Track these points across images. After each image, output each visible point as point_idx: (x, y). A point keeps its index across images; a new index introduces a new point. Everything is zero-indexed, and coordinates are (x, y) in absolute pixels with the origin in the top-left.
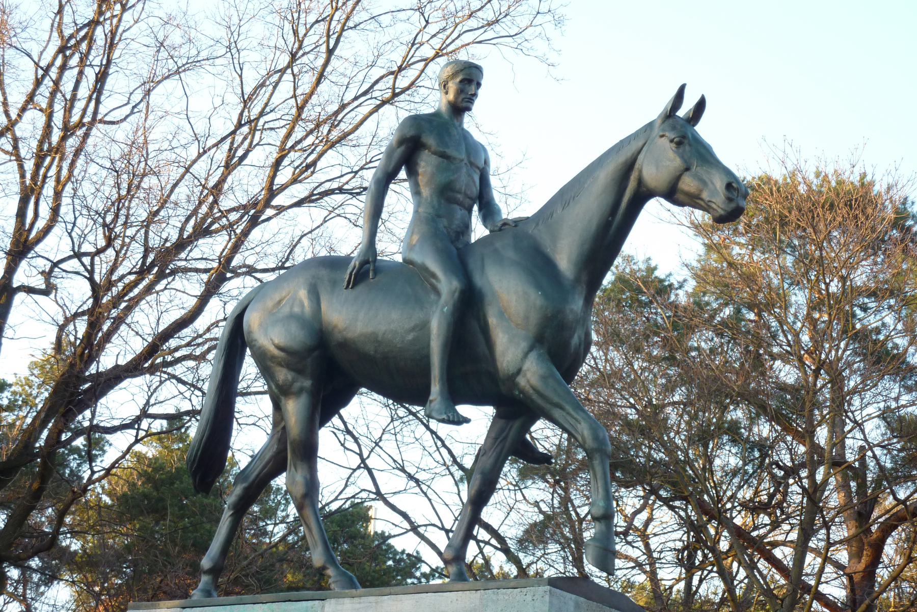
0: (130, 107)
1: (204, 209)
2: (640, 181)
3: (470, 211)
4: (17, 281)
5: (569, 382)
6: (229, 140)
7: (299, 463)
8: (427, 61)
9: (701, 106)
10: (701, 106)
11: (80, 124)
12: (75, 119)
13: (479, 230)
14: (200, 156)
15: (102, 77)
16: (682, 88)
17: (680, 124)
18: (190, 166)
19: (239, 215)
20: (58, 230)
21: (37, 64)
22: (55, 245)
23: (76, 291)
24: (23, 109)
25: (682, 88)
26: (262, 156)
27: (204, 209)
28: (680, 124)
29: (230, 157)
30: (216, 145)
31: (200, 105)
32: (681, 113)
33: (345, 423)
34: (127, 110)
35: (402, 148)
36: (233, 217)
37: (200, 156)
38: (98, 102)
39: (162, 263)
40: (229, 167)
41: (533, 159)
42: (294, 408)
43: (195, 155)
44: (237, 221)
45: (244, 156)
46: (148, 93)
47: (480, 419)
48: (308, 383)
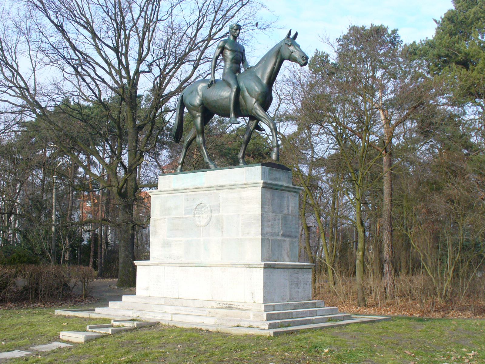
0: (168, 15)
2: (281, 56)
4: (140, 70)
6: (197, 21)
7: (200, 136)
8: (219, 24)
9: (296, 35)
10: (296, 35)
13: (242, 70)
16: (290, 30)
17: (291, 39)
18: (186, 31)
19: (202, 44)
20: (149, 55)
21: (140, 7)
22: (149, 59)
23: (156, 71)
24: (138, 18)
25: (290, 30)
26: (208, 24)
28: (291, 39)
29: (198, 26)
30: (193, 23)
31: (187, 12)
32: (291, 36)
36: (200, 44)
39: (181, 60)
40: (198, 30)
43: (187, 28)
44: (201, 46)
45: (202, 25)
48: (200, 114)
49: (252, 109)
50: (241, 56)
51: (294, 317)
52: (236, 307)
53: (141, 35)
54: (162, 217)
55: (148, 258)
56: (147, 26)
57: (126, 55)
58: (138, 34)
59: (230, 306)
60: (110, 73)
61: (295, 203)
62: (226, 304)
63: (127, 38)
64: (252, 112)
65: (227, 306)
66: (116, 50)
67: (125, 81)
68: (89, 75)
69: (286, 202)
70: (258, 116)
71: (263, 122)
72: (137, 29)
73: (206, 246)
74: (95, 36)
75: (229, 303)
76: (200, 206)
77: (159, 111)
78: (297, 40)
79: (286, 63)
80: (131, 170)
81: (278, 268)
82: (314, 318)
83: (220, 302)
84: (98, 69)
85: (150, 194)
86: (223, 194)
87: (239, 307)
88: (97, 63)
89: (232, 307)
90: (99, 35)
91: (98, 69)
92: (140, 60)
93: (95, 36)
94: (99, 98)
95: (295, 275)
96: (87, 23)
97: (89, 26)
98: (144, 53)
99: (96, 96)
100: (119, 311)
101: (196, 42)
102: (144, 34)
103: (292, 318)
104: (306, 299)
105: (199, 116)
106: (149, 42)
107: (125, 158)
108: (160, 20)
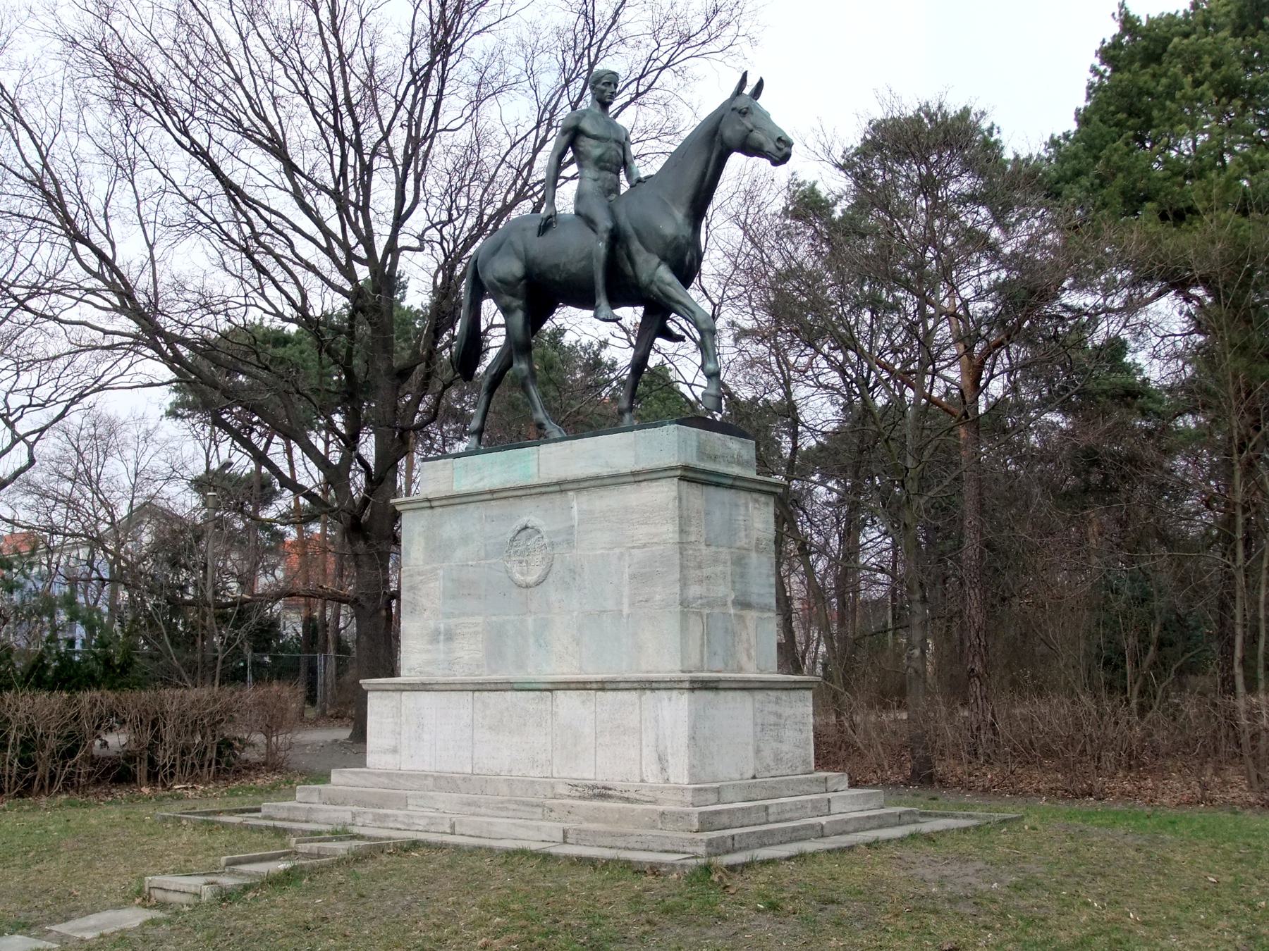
1: (520, 182)
2: (723, 142)
3: (618, 174)
5: (687, 288)
9: (760, 85)
10: (760, 85)
11: (425, 138)
12: (422, 133)
13: (625, 186)
14: (512, 147)
15: (437, 105)
16: (745, 75)
20: (421, 206)
25: (745, 75)
27: (520, 182)
32: (747, 91)
33: (34, 432)
34: (462, 120)
35: (567, 136)
37: (512, 147)
38: (437, 120)
41: (656, 131)
42: (519, 317)
46: (476, 108)
47: (631, 315)
48: (520, 302)
49: (652, 282)
50: (621, 152)
51: (771, 818)
52: (619, 794)
53: (399, 161)
54: (428, 567)
55: (392, 671)
56: (414, 142)
57: (365, 209)
58: (395, 166)
59: (604, 791)
60: (329, 251)
61: (767, 522)
62: (594, 787)
63: (367, 169)
64: (651, 292)
65: (596, 791)
66: (339, 199)
67: (363, 272)
68: (278, 258)
69: (741, 518)
70: (665, 300)
71: (679, 314)
72: (390, 150)
73: (573, 659)
74: (291, 169)
75: (600, 784)
76: (524, 533)
77: (446, 337)
78: (762, 101)
79: (736, 161)
80: (381, 479)
81: (725, 689)
82: (823, 820)
83: (576, 782)
84: (297, 239)
85: (398, 508)
86: (578, 504)
87: (626, 795)
88: (296, 229)
89: (610, 797)
90: (301, 167)
91: (297, 239)
92: (400, 219)
93: (291, 169)
94: (303, 310)
95: (773, 707)
96: (274, 138)
97: (277, 148)
98: (407, 205)
99: (294, 305)
100: (316, 808)
101: (530, 182)
102: (406, 165)
103: (767, 822)
104: (799, 770)
105: (518, 307)
106: (417, 180)
107: (368, 447)
108: (445, 129)
